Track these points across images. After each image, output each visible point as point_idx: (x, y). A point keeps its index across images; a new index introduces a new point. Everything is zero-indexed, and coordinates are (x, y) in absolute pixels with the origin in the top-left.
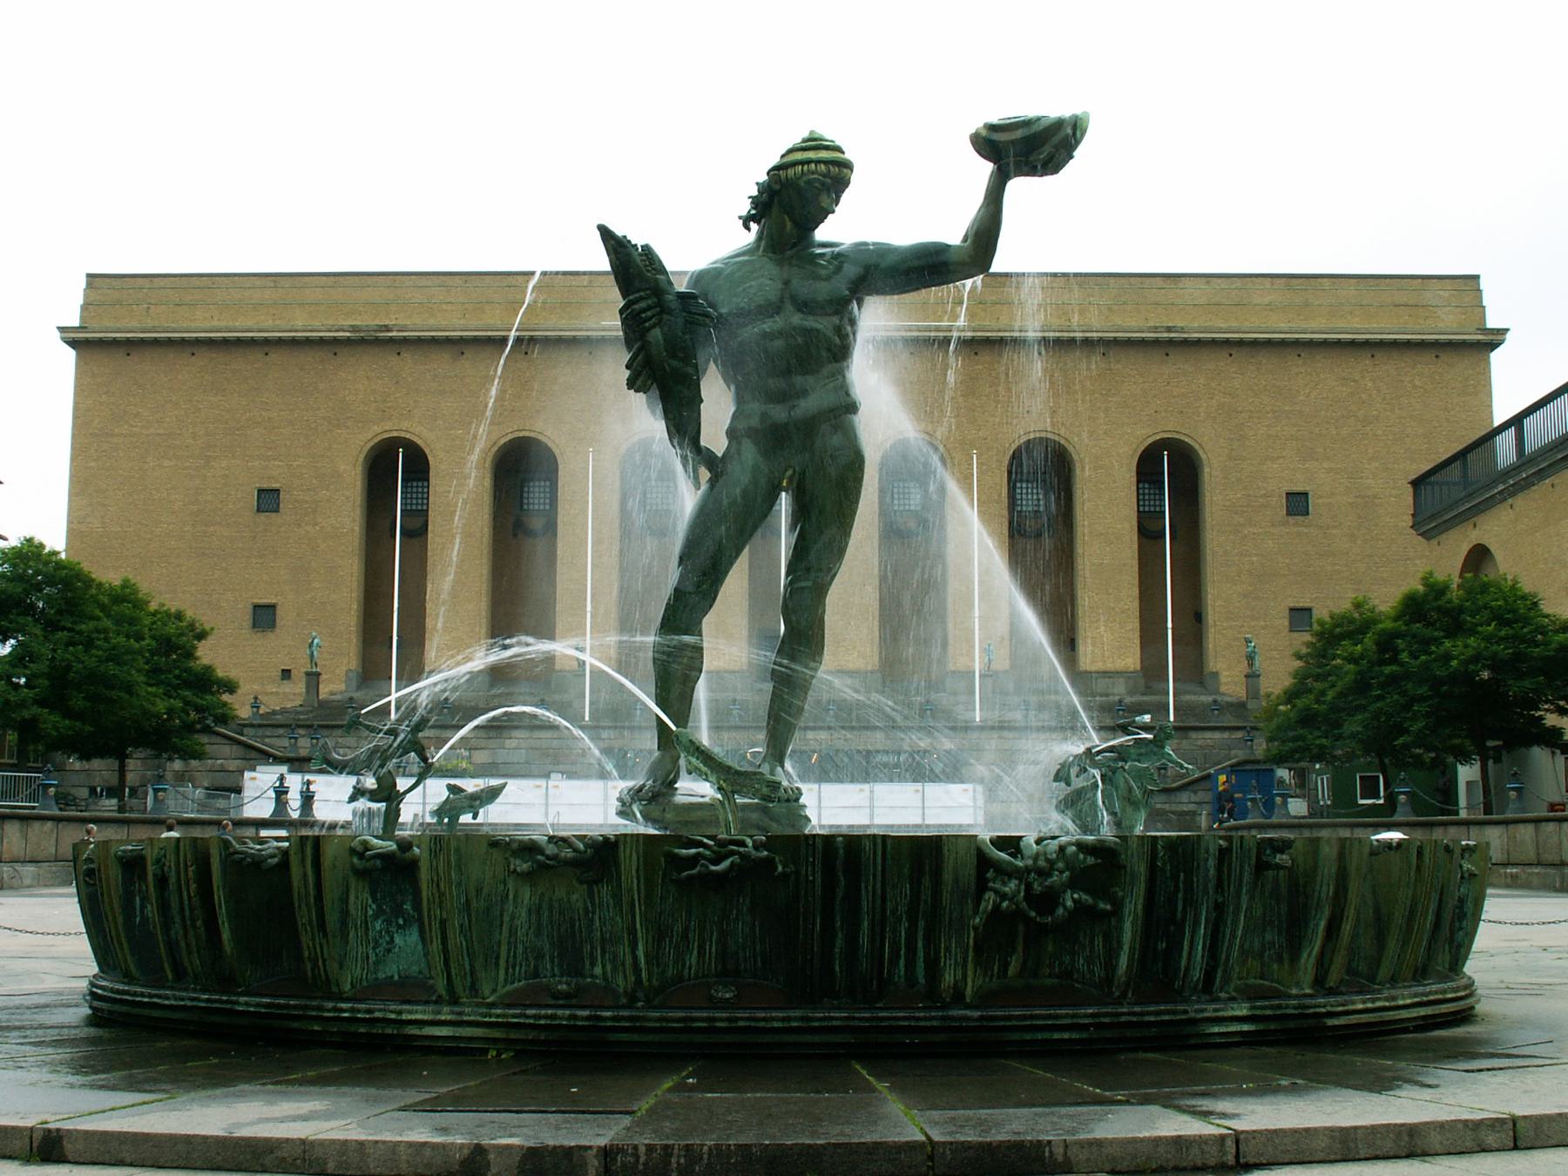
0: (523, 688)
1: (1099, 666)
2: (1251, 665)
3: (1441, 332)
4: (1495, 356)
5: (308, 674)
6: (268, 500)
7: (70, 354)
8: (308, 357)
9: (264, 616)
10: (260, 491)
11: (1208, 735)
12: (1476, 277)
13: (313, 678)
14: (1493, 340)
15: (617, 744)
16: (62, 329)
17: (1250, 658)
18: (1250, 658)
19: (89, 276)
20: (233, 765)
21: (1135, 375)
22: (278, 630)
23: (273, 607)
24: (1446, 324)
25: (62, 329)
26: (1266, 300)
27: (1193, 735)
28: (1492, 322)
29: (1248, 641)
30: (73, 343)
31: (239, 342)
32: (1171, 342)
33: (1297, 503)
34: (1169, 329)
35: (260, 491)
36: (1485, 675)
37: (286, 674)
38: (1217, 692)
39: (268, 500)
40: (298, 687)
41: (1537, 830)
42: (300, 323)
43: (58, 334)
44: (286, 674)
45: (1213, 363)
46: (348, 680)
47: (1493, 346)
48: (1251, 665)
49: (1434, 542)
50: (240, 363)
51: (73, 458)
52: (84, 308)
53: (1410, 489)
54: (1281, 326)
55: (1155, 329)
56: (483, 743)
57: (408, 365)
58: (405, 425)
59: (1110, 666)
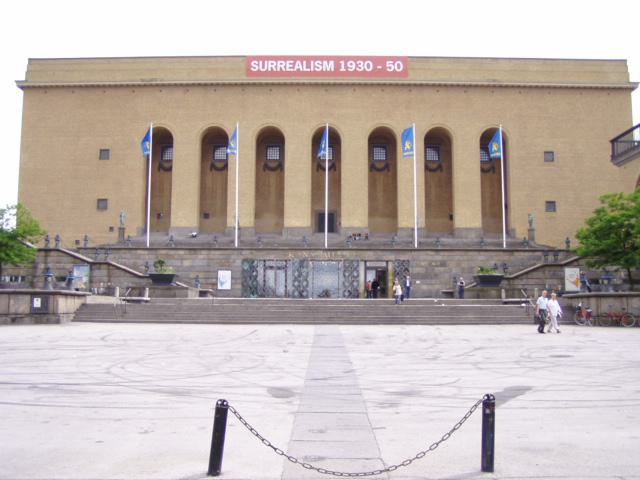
0: (156, 220)
1: (463, 226)
2: (531, 225)
3: (603, 84)
4: (633, 93)
5: (120, 229)
6: (104, 154)
7: (21, 92)
8: (121, 93)
9: (558, 332)
10: (101, 150)
11: (522, 254)
12: (625, 61)
13: (122, 230)
14: (632, 88)
15: (250, 257)
16: (17, 82)
17: (530, 222)
18: (530, 222)
19: (30, 60)
20: (68, 266)
21: (479, 100)
22: (108, 210)
23: (106, 200)
24: (612, 80)
25: (17, 82)
26: (535, 69)
27: (516, 254)
28: (632, 79)
29: (529, 215)
30: (22, 88)
31: (93, 86)
32: (494, 86)
33: (549, 156)
34: (494, 81)
35: (101, 150)
36: (418, 282)
37: (111, 229)
38: (514, 237)
39: (104, 154)
40: (115, 234)
41: (91, 269)
42: (119, 79)
43: (15, 84)
44: (111, 229)
45: (513, 95)
46: (138, 232)
47: (633, 89)
48: (531, 225)
49: (622, 167)
50: (94, 95)
51: (22, 137)
52: (28, 73)
53: (610, 145)
54: (542, 81)
55: (488, 81)
56: (188, 256)
57: (164, 95)
58: (163, 121)
59: (468, 226)
